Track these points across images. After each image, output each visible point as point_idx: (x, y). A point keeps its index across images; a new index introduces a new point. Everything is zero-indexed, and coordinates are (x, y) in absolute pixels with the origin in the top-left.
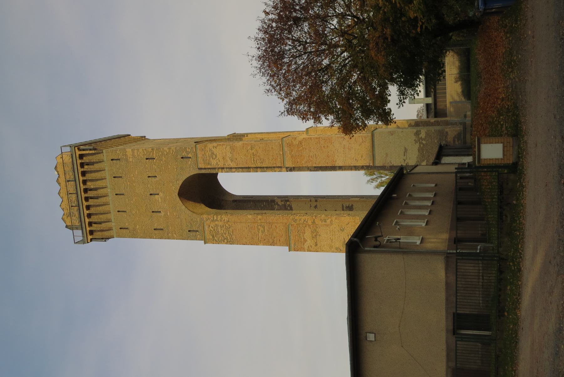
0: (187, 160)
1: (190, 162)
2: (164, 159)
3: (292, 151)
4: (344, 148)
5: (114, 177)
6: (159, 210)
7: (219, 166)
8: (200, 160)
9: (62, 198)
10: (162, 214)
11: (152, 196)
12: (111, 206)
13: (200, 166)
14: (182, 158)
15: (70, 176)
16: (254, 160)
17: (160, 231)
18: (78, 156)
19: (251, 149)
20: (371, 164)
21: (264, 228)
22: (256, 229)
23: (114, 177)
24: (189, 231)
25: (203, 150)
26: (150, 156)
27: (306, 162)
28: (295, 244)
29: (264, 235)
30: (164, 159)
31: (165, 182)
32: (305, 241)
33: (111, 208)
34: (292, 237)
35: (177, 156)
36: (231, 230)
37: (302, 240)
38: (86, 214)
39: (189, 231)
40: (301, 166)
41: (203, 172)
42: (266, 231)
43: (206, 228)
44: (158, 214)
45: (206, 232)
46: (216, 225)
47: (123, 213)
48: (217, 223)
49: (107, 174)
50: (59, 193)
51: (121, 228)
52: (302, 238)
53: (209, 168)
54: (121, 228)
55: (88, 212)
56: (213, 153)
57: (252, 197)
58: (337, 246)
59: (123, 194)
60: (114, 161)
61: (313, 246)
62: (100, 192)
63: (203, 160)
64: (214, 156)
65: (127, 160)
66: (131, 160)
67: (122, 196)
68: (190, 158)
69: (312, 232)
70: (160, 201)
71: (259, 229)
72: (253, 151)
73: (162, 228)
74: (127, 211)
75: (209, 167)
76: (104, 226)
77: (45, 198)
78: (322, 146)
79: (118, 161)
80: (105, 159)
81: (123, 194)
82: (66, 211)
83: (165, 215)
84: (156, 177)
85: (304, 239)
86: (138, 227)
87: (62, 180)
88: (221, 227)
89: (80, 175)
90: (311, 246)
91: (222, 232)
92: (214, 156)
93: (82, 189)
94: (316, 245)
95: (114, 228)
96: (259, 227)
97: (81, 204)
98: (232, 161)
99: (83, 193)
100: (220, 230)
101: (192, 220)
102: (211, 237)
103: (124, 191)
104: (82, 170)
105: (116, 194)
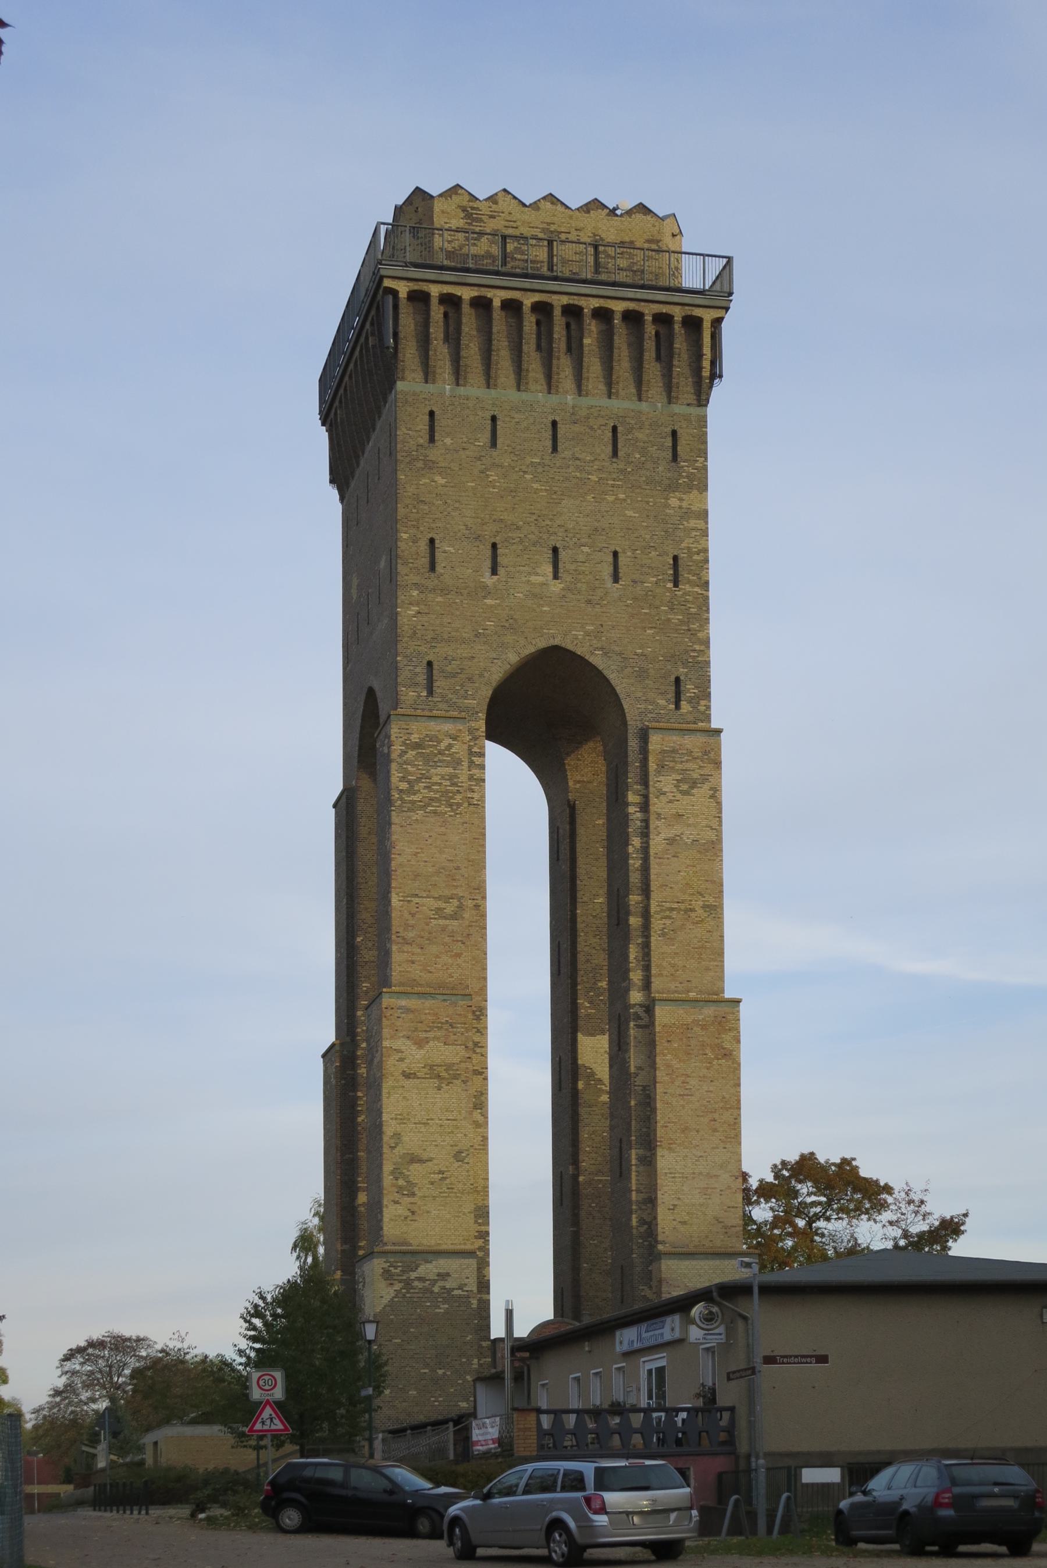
0: (671, 695)
1: (662, 702)
2: (676, 618)
3: (704, 1027)
4: (709, 1176)
5: (615, 429)
6: (501, 571)
7: (653, 800)
8: (674, 740)
9: (535, 206)
10: (489, 580)
11: (549, 554)
12: (513, 395)
13: (655, 741)
14: (677, 680)
15: (618, 265)
16: (672, 909)
17: (425, 561)
18: (698, 312)
19: (704, 907)
20: (660, 1247)
21: (454, 916)
22: (447, 892)
23: (615, 429)
24: (430, 664)
25: (706, 753)
26: (684, 574)
27: (668, 1066)
28: (408, 1010)
29: (431, 914)
30: (676, 618)
31: (598, 609)
32: (420, 1044)
33: (506, 393)
34: (429, 1003)
35: (685, 664)
36: (443, 808)
37: (423, 1035)
38: (489, 294)
39: (430, 664)
40: (658, 1049)
41: (633, 744)
42: (441, 922)
43: (448, 727)
44: (488, 563)
45: (432, 724)
46: (459, 762)
47: (488, 434)
48: (465, 764)
49: (623, 404)
50: (551, 198)
51: (432, 414)
52: (431, 1035)
53: (644, 762)
54: (432, 414)
55: (497, 303)
56: (694, 784)
57: (343, 640)
58: (405, 1139)
59: (555, 449)
60: (669, 442)
61: (403, 1066)
62: (564, 366)
63: (674, 751)
64: (684, 787)
65: (672, 487)
66: (674, 502)
67: (549, 443)
68: (678, 707)
69: (449, 1067)
70: (533, 578)
71: (447, 899)
72: (700, 911)
73: (439, 569)
74: (495, 453)
75: (652, 766)
76: (440, 350)
77: (542, 147)
78: (716, 1116)
79: (669, 455)
80: (677, 408)
81: (555, 449)
82: (485, 208)
83: (485, 587)
84: (616, 578)
85: (427, 1040)
86: (440, 480)
87: (596, 223)
88: (452, 777)
89: (632, 306)
90: (401, 1060)
91: (436, 779)
92: (684, 787)
93: (582, 302)
94: (407, 1076)
95: (430, 387)
96: (455, 902)
97: (527, 286)
98: (671, 841)
99: (565, 300)
100: (439, 770)
101: (470, 679)
102: (415, 738)
103: (567, 454)
104: (649, 318)
105: (554, 424)
